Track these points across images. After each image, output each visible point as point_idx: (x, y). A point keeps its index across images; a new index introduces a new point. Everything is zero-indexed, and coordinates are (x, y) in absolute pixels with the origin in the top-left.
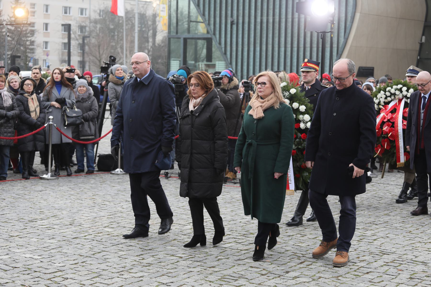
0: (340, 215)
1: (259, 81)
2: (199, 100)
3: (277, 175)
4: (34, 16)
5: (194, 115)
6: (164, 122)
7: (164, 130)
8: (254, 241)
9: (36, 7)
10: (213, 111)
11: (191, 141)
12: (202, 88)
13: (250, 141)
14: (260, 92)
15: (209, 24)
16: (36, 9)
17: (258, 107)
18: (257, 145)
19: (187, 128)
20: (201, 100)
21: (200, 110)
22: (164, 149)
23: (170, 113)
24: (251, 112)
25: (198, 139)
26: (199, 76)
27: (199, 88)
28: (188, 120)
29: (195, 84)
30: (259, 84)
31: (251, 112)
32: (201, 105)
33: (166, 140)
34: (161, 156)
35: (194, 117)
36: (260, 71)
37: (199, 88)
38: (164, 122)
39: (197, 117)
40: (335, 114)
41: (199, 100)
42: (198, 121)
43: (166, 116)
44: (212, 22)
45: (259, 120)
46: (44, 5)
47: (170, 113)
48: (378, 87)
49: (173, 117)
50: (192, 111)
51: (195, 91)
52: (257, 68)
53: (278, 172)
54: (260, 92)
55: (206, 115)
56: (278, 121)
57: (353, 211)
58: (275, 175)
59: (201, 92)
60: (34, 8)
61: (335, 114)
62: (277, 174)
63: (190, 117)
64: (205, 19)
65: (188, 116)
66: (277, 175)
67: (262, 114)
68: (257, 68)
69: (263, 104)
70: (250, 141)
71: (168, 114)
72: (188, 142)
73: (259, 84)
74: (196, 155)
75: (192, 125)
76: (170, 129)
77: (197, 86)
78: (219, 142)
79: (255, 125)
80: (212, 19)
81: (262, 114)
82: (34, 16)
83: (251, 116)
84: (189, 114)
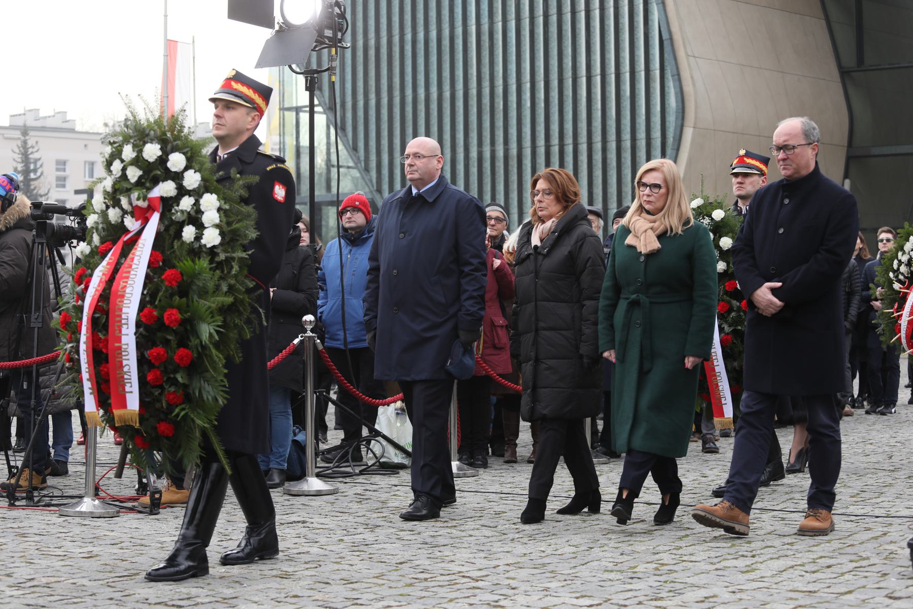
0: (636, 500)
1: (644, 180)
2: (549, 224)
3: (689, 362)
4: (64, 186)
5: (540, 253)
6: (463, 281)
7: (464, 297)
8: (679, 507)
9: (67, 167)
10: (577, 242)
11: (536, 305)
12: (558, 199)
13: (634, 296)
14: (649, 202)
15: (367, 169)
16: (68, 172)
17: (646, 231)
18: (651, 303)
19: (527, 279)
20: (555, 224)
21: (551, 242)
22: (463, 336)
23: (475, 261)
24: (630, 240)
25: (548, 300)
26: (552, 175)
27: (552, 197)
28: (530, 265)
29: (544, 190)
30: (645, 185)
31: (630, 240)
32: (554, 232)
33: (469, 318)
34: (458, 350)
35: (540, 258)
36: (648, 159)
37: (552, 197)
38: (463, 281)
39: (545, 256)
40: (781, 231)
41: (549, 224)
42: (547, 264)
43: (467, 269)
44: (373, 164)
45: (651, 255)
46: (85, 162)
47: (475, 261)
48: (509, 311)
49: (480, 271)
50: (536, 247)
51: (543, 205)
52: (642, 153)
53: (692, 356)
54: (649, 202)
55: (564, 250)
56: (682, 255)
57: (832, 427)
58: (686, 361)
59: (555, 208)
60: (64, 170)
61: (781, 231)
62: (691, 359)
63: (532, 257)
64: (359, 158)
65: (528, 256)
66: (689, 362)
67: (656, 245)
68: (642, 153)
69: (656, 225)
70: (634, 296)
71: (471, 264)
72: (530, 307)
73: (645, 185)
74: (547, 333)
75: (537, 273)
76: (475, 294)
77: (548, 194)
78: (587, 303)
79: (643, 265)
80: (373, 157)
81: (656, 245)
82: (64, 186)
83: (632, 247)
84: (531, 252)
